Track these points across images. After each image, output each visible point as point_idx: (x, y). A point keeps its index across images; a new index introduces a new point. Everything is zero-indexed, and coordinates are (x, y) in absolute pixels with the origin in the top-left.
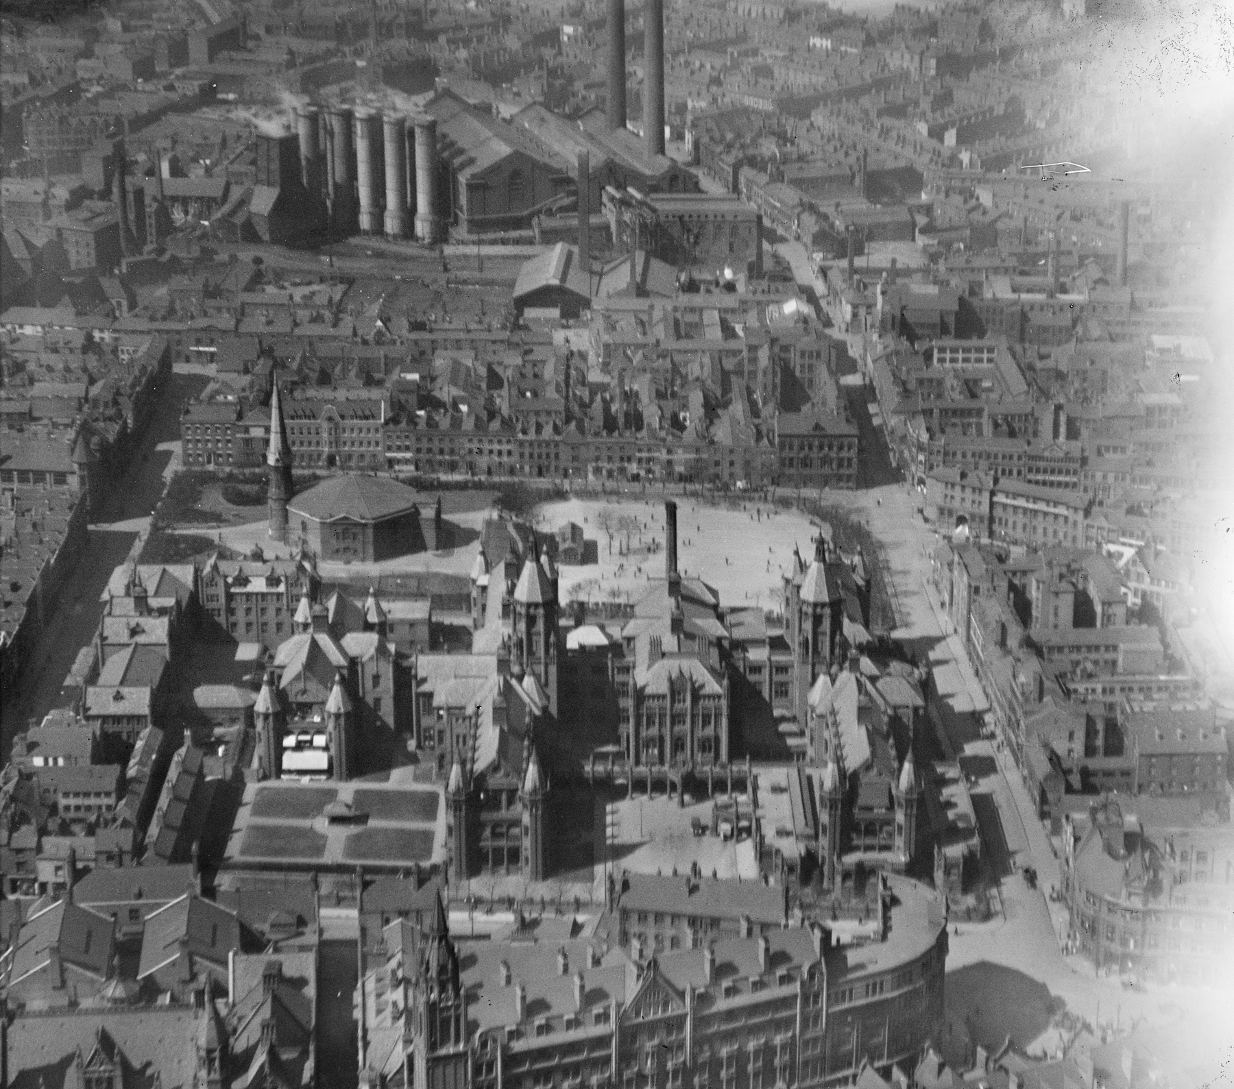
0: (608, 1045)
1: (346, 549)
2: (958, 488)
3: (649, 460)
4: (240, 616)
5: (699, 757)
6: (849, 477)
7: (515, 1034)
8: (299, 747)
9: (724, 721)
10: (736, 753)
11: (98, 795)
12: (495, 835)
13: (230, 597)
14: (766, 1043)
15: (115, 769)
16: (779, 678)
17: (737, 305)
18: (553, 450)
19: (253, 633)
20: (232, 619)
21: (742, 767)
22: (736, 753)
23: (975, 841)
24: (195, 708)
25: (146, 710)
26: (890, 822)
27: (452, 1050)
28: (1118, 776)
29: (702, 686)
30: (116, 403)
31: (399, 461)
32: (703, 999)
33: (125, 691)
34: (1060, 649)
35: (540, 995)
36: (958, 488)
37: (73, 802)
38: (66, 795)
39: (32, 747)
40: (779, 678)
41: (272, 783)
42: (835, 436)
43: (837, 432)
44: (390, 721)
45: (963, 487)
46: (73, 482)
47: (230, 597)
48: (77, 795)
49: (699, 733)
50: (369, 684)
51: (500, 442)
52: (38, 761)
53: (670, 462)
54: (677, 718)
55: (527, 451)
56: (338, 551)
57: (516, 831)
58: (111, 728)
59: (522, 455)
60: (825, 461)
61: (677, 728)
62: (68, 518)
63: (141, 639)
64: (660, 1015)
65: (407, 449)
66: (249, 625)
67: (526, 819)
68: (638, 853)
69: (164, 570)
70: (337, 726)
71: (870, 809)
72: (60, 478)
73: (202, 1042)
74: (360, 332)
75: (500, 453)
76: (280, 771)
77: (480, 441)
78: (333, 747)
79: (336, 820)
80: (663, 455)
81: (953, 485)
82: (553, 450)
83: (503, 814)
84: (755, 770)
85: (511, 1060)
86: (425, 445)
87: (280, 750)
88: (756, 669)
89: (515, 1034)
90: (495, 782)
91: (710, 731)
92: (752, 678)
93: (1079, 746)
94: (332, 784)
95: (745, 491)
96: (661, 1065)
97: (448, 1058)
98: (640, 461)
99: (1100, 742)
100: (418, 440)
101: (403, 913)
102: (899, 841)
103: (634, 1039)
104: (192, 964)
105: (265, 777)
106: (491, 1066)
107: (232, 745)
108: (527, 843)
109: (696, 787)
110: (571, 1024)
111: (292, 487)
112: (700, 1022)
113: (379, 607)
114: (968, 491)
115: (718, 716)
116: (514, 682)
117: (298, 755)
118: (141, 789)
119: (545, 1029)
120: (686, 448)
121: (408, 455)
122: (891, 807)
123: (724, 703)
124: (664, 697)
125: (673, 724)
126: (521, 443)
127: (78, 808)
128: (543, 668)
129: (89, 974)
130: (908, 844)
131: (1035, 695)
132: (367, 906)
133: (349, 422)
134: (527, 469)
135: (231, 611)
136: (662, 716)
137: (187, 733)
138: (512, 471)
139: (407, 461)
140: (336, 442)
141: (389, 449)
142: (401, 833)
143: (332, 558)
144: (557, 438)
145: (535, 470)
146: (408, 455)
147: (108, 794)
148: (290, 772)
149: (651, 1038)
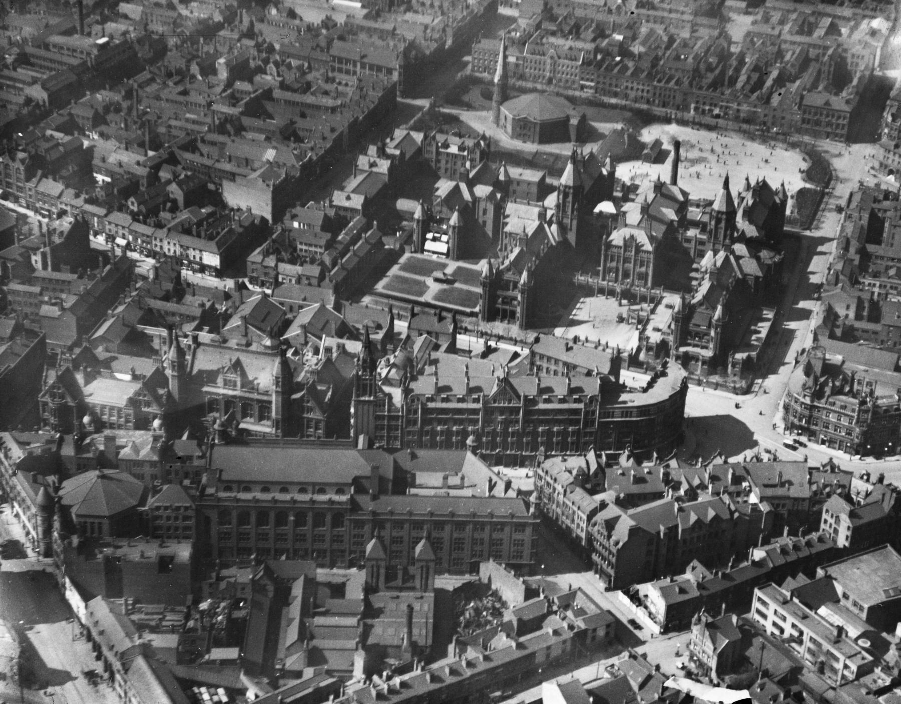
0: (478, 414)
1: (524, 135)
2: (892, 153)
3: (727, 107)
4: (443, 164)
5: (636, 282)
6: (842, 136)
7: (431, 399)
8: (435, 239)
9: (651, 265)
10: (655, 285)
11: (316, 246)
12: (503, 303)
13: (438, 153)
14: (549, 429)
15: (328, 236)
16: (700, 247)
17: (851, 15)
18: (672, 94)
19: (449, 173)
20: (439, 165)
21: (657, 292)
22: (655, 285)
23: (754, 354)
24: (397, 210)
25: (360, 207)
26: (708, 334)
27: (367, 399)
28: (870, 333)
29: (643, 245)
30: (444, 30)
31: (587, 87)
32: (534, 402)
33: (352, 195)
34: (882, 258)
35: (446, 384)
36: (892, 153)
37: (304, 247)
38: (301, 243)
39: (294, 217)
40: (700, 247)
41: (419, 256)
42: (838, 111)
43: (838, 108)
44: (490, 233)
45: (895, 154)
46: (396, 76)
47: (438, 153)
48: (306, 244)
49: (638, 269)
50: (481, 213)
51: (643, 84)
52: (296, 224)
53: (738, 110)
54: (626, 260)
55: (658, 92)
56: (520, 135)
57: (515, 303)
58: (342, 213)
59: (655, 94)
60: (829, 124)
61: (626, 265)
62: (380, 95)
63: (375, 169)
64: (506, 405)
65: (592, 80)
66: (447, 170)
67: (519, 298)
68: (583, 326)
69: (409, 134)
70: (453, 232)
71: (699, 326)
72: (390, 71)
73: (274, 373)
74: (608, 4)
75: (643, 91)
76: (423, 250)
77: (632, 82)
78: (451, 241)
79: (437, 280)
80: (735, 106)
81: (890, 151)
82: (672, 94)
83: (510, 293)
84: (665, 294)
85: (426, 411)
86: (601, 79)
87: (424, 240)
88: (688, 240)
89: (431, 399)
90: (508, 276)
91: (643, 269)
92: (686, 245)
93: (852, 314)
94: (448, 261)
95: (778, 133)
96: (505, 430)
97: (365, 401)
98: (721, 107)
99: (865, 313)
100: (598, 76)
101: (429, 333)
102: (711, 345)
103: (492, 414)
104: (306, 337)
105: (416, 252)
106: (416, 412)
107: (406, 233)
108: (518, 310)
109: (629, 296)
110: (460, 400)
111: (505, 98)
112: (527, 413)
113: (506, 171)
114: (897, 156)
115: (648, 262)
116: (546, 226)
117: (433, 243)
118: (340, 247)
119: (446, 400)
120: (749, 104)
121: (592, 84)
122: (709, 327)
123: (652, 256)
124: (620, 247)
125: (624, 262)
126: (655, 87)
127: (306, 251)
128: (569, 221)
129: (258, 332)
130: (715, 347)
131: (833, 281)
132: (412, 326)
133: (561, 61)
134: (657, 101)
135: (438, 161)
136: (619, 257)
137: (375, 223)
138: (648, 102)
139: (591, 87)
140: (553, 71)
141: (582, 79)
142: (468, 292)
143: (517, 138)
144: (676, 87)
145: (661, 103)
146: (592, 84)
147: (321, 247)
148: (429, 251)
149: (501, 415)
